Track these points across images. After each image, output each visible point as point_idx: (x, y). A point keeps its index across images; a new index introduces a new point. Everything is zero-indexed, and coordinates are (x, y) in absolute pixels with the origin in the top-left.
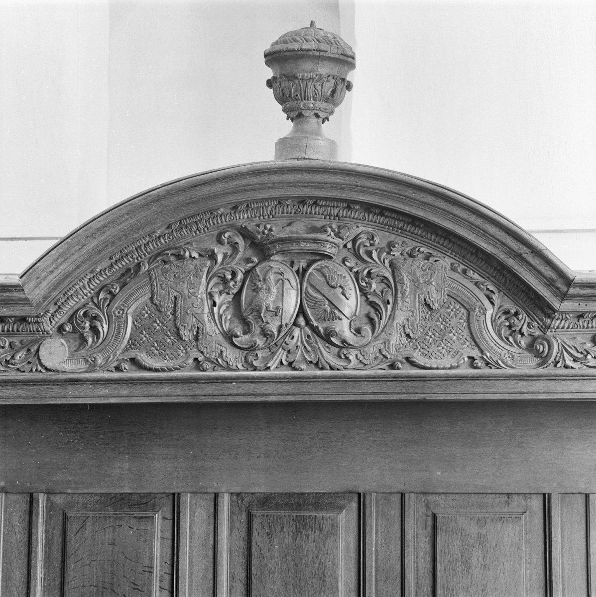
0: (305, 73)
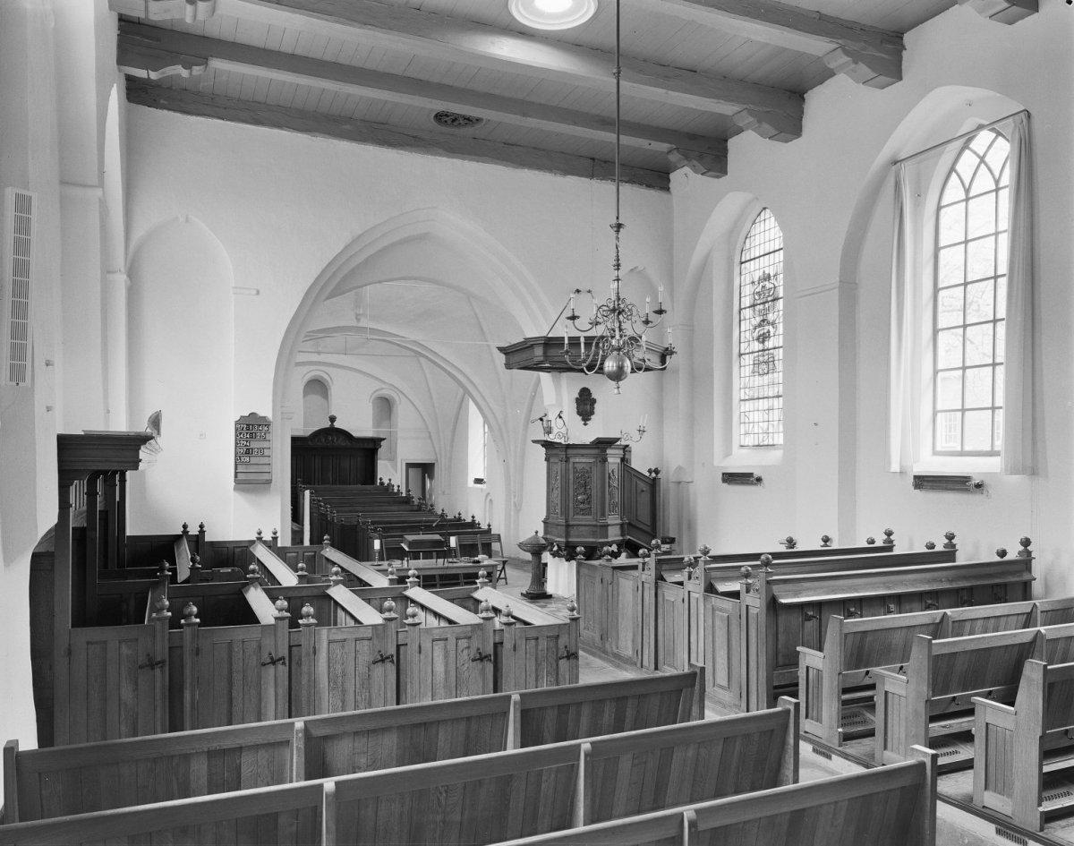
0: (333, 419)
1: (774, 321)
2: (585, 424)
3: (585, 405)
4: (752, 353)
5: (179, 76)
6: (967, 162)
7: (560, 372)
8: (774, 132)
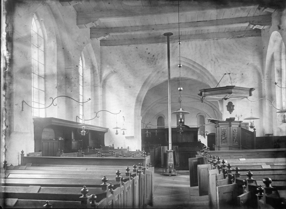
2: (231, 114)
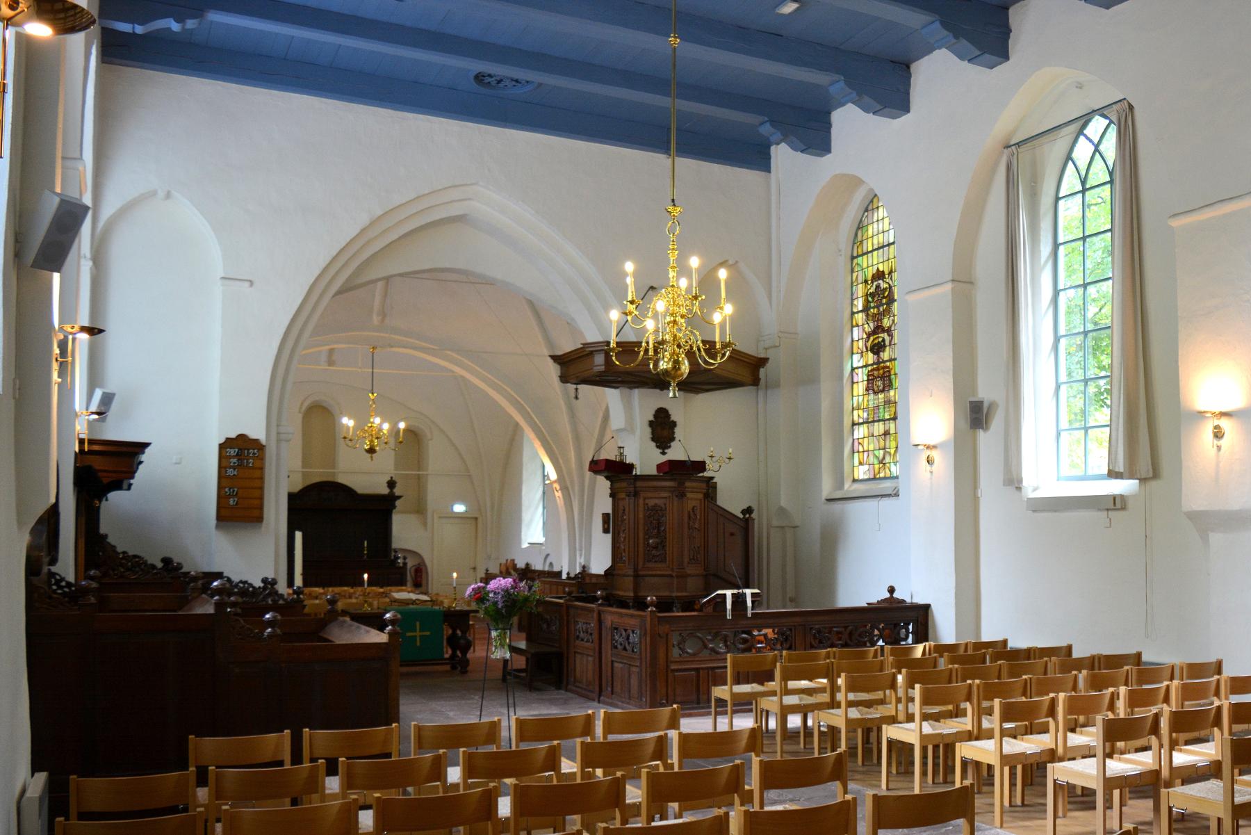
1: (889, 328)
3: (662, 429)
4: (866, 366)
5: (169, 29)
6: (1083, 151)
7: (631, 388)
8: (879, 107)
